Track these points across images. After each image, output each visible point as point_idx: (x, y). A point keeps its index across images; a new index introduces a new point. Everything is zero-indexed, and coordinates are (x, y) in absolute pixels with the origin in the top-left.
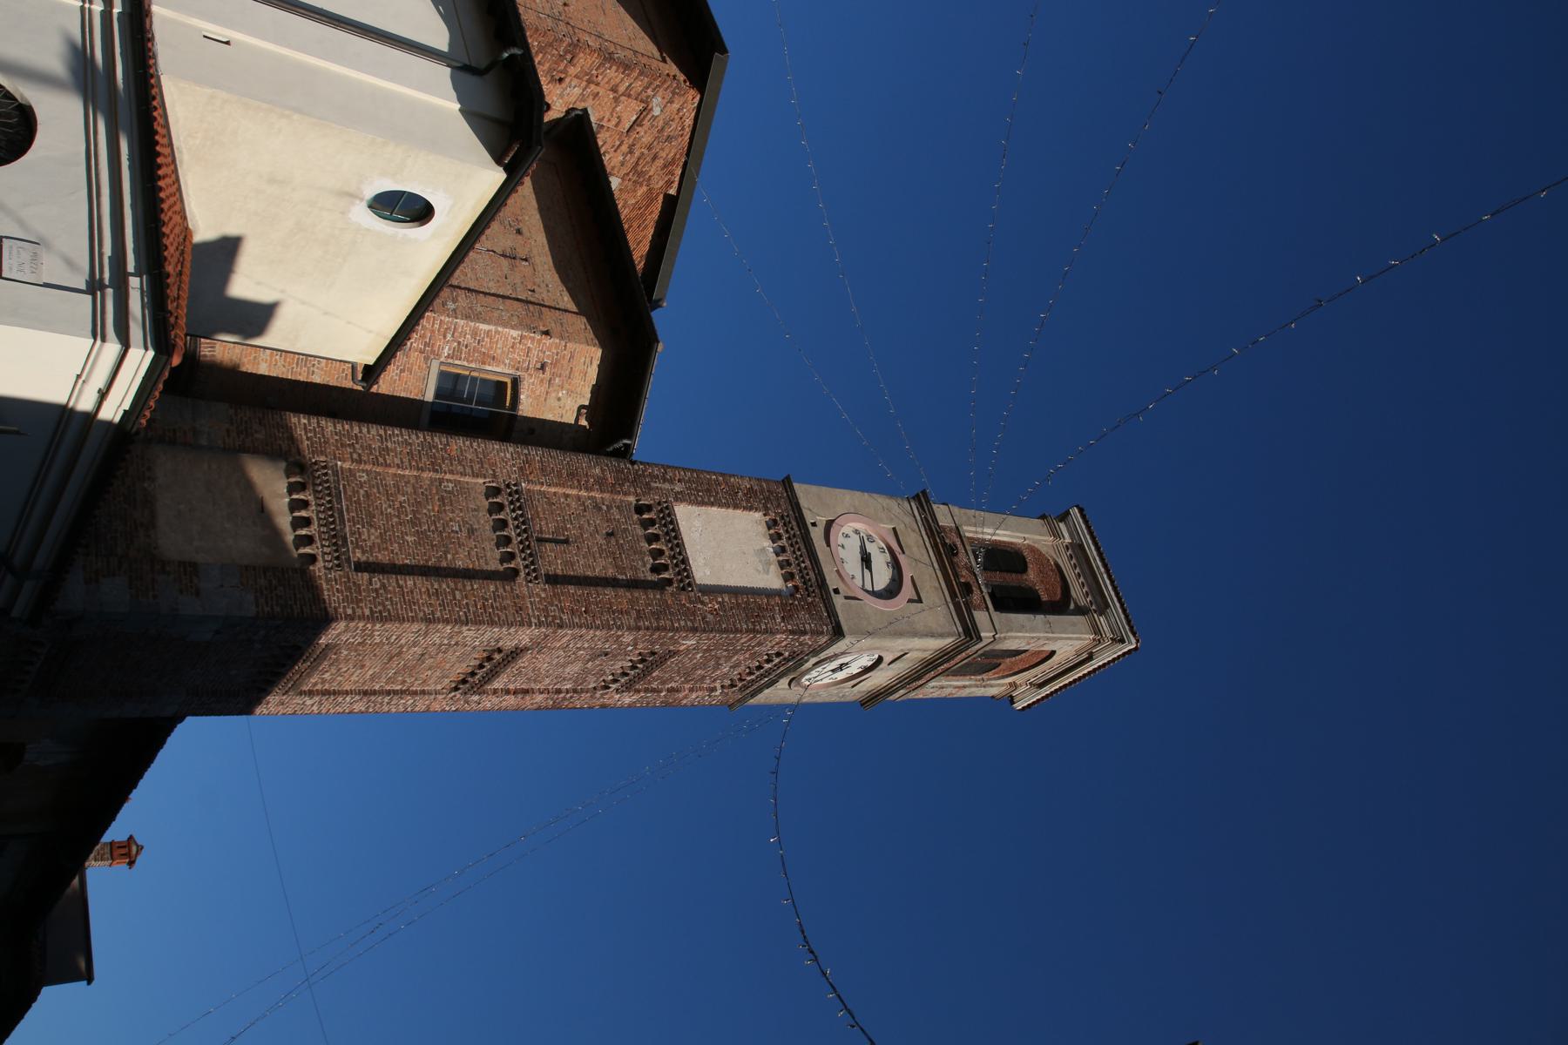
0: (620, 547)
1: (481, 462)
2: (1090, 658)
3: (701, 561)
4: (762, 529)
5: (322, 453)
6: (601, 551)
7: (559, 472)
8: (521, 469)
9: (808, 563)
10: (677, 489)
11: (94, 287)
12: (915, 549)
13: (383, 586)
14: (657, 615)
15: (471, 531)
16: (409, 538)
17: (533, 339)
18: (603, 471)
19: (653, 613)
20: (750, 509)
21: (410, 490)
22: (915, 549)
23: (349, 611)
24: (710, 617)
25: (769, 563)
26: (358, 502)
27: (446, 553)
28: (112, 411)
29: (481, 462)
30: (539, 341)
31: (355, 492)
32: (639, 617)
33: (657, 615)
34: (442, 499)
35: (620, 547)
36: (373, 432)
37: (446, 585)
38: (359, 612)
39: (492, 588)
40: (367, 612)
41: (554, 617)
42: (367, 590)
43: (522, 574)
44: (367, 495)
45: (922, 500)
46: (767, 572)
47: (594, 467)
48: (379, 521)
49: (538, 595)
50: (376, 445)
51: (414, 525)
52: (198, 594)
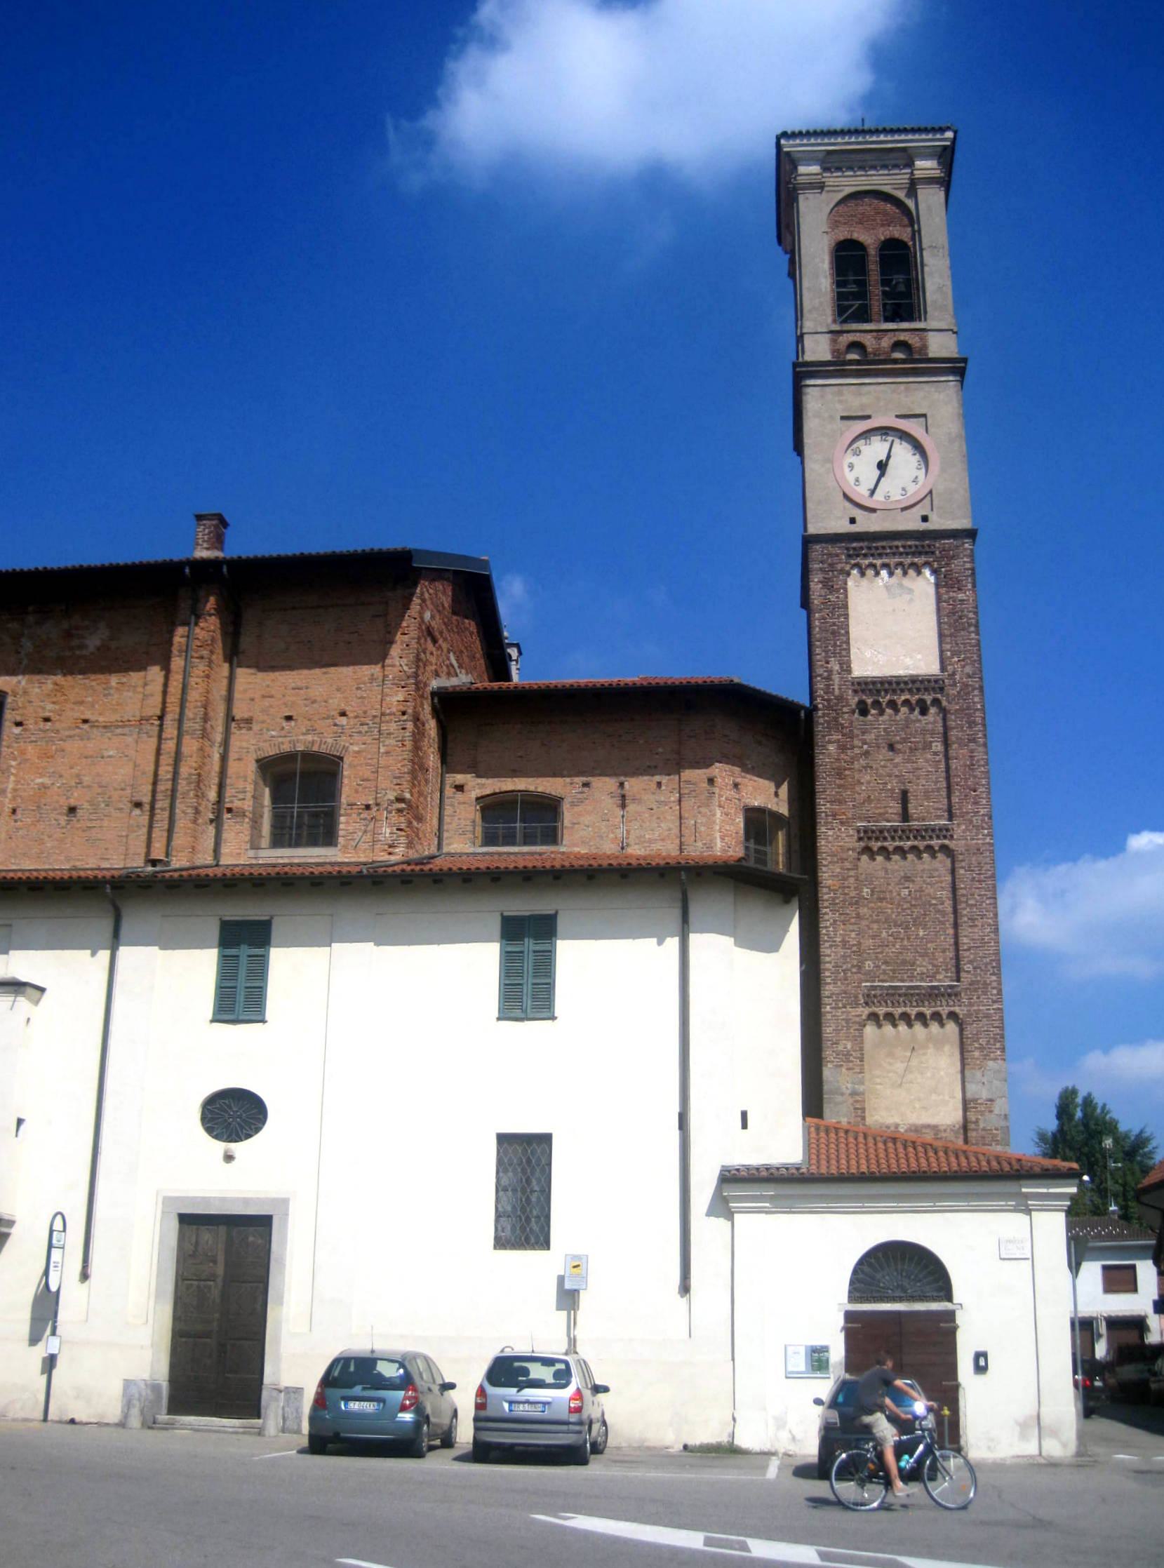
0: (904, 740)
1: (843, 860)
2: (924, 820)
3: (908, 661)
4: (864, 582)
5: (856, 997)
6: (908, 761)
7: (840, 786)
8: (842, 823)
9: (899, 543)
10: (837, 667)
11: (1028, 1212)
12: (865, 400)
13: (970, 962)
14: (972, 724)
15: (907, 878)
16: (921, 933)
17: (721, 796)
18: (830, 742)
19: (970, 727)
20: (846, 590)
21: (875, 926)
22: (865, 400)
23: (995, 992)
24: (968, 669)
25: (901, 585)
26: (894, 971)
27: (931, 905)
28: (181, 631)
29: (843, 860)
30: (721, 789)
31: (884, 972)
32: (974, 740)
33: (972, 724)
34: (881, 900)
35: (904, 740)
36: (828, 951)
37: (965, 912)
38: (994, 984)
39: (962, 871)
40: (994, 978)
41: (983, 821)
42: (976, 976)
43: (946, 842)
44: (886, 963)
45: (802, 373)
46: (911, 591)
47: (828, 752)
48: (909, 956)
49: (964, 831)
50: (842, 952)
51: (907, 927)
52: (991, 1100)
